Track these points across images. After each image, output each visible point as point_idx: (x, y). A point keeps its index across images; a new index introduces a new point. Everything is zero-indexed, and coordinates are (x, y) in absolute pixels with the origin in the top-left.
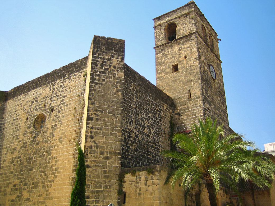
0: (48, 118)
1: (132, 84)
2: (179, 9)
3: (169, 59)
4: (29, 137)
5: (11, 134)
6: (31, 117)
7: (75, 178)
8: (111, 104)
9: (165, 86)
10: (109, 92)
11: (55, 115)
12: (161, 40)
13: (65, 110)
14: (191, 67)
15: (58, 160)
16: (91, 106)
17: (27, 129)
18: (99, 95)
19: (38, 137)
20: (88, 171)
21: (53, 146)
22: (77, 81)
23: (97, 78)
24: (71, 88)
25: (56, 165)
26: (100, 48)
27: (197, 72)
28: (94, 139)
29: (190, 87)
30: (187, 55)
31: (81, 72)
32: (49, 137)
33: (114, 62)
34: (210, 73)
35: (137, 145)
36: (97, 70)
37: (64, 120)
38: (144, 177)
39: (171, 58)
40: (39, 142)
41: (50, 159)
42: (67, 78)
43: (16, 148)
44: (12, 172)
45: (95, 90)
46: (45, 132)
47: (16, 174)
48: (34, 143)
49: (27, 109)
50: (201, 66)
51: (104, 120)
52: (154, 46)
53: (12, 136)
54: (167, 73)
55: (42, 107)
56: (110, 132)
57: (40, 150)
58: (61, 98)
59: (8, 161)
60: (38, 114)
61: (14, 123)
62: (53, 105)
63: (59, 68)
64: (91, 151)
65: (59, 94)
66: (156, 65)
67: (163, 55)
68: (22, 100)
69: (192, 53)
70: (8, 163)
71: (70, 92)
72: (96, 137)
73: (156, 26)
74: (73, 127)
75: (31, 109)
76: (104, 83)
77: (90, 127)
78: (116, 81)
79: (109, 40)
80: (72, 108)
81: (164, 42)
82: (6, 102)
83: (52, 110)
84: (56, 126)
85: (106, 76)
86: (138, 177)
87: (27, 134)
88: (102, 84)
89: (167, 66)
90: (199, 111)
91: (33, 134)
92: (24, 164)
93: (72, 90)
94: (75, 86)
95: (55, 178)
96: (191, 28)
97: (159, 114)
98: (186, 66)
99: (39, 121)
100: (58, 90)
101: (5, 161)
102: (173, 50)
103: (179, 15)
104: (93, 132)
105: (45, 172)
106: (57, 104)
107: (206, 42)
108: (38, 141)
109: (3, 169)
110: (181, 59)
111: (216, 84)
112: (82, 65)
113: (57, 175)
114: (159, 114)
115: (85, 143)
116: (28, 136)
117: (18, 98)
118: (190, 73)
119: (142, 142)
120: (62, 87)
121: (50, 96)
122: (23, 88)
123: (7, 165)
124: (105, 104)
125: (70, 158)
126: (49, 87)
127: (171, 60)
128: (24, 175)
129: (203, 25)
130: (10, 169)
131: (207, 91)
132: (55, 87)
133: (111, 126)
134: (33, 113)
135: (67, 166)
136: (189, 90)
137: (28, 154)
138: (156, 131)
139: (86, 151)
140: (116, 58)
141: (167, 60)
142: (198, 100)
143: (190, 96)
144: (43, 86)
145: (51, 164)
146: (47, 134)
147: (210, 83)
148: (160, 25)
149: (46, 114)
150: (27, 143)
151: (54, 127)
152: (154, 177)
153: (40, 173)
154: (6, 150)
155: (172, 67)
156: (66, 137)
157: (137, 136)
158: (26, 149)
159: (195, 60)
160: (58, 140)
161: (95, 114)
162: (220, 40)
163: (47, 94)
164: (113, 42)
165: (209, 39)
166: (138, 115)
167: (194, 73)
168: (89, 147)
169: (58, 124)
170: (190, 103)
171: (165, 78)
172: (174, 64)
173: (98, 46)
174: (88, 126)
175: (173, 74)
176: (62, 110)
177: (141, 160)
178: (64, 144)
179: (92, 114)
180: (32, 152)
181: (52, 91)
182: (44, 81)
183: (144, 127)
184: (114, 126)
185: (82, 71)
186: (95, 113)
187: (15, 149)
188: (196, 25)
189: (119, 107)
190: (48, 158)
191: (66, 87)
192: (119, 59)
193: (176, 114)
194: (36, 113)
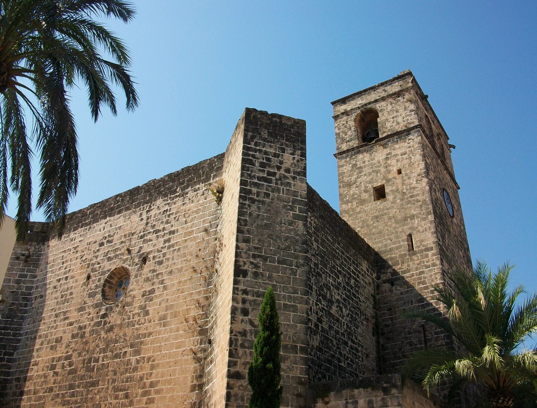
0: (136, 276)
1: (309, 213)
2: (382, 84)
3: (365, 175)
4: (91, 316)
5: (52, 310)
6: (97, 275)
7: (197, 404)
8: (282, 243)
9: (359, 227)
10: (279, 219)
11: (150, 271)
12: (349, 141)
13: (173, 259)
14: (412, 191)
15: (158, 365)
16: (243, 245)
17: (86, 299)
18: (258, 225)
19: (112, 315)
20: (239, 386)
21: (145, 334)
22: (201, 202)
23: (254, 190)
24: (187, 215)
25: (153, 375)
26: (257, 132)
27: (425, 200)
28: (250, 317)
29: (411, 228)
30: (403, 167)
31: (210, 184)
32: (136, 316)
33: (287, 161)
34: (444, 205)
35: (321, 338)
36: (253, 174)
37: (172, 280)
38: (364, 400)
39: (370, 174)
40: (113, 326)
41: (138, 362)
42: (179, 196)
43: (61, 337)
44: (51, 390)
45: (251, 214)
46: (128, 304)
47: (58, 394)
48: (104, 328)
49: (89, 257)
50: (430, 189)
51: (270, 277)
52: (336, 152)
53: (54, 313)
54: (362, 202)
55: (122, 254)
56: (282, 302)
57: (116, 341)
58: (164, 235)
59: (42, 366)
60: (113, 267)
61: (58, 287)
62: (146, 248)
63: (162, 176)
64: (244, 341)
65: (161, 228)
66: (340, 187)
67: (352, 168)
68: (77, 240)
69: (413, 164)
70: (43, 370)
71: (186, 222)
72: (254, 311)
73: (338, 116)
74: (192, 294)
75: (96, 257)
76: (267, 200)
77: (241, 290)
78: (291, 198)
79: (276, 119)
80: (191, 255)
81: (355, 143)
82: (43, 244)
83: (144, 260)
84: (152, 291)
85: (270, 186)
86: (350, 401)
87: (87, 309)
88: (263, 203)
89: (362, 189)
90: (431, 276)
91: (100, 310)
92: (78, 373)
93: (189, 219)
94: (196, 212)
95: (150, 403)
96: (408, 119)
97: (356, 280)
98: (400, 189)
99: (114, 283)
100: (159, 220)
101: (36, 364)
102: (374, 159)
103: (383, 94)
104: (248, 302)
105: (125, 390)
106: (156, 248)
107: (434, 146)
108: (111, 324)
109: (31, 381)
110: (390, 176)
111: (455, 227)
112: (211, 169)
113: (154, 398)
114: (356, 280)
115: (232, 323)
116: (90, 314)
117: (69, 236)
118: (409, 202)
119: (329, 333)
120: (168, 213)
121: (140, 232)
122: (82, 217)
123: (41, 373)
124: (270, 244)
125: (185, 360)
126: (139, 214)
127: (371, 177)
128: (77, 396)
129: (426, 117)
130: (45, 382)
131: (443, 237)
132: (152, 213)
133: (284, 289)
134: (102, 267)
135: (179, 378)
136: (410, 236)
137: (88, 352)
138: (352, 312)
139: (234, 341)
140: (291, 154)
141: (362, 177)
142: (430, 253)
143: (411, 246)
144: (125, 211)
145: (140, 373)
146: (131, 310)
147: (446, 222)
148: (346, 113)
149: (130, 268)
150: (87, 327)
151: (149, 295)
152: (388, 399)
153: (114, 391)
154: (40, 342)
155: (372, 191)
156: (175, 315)
157: (320, 320)
158: (84, 340)
159: (419, 178)
160: (157, 322)
161: (252, 263)
162: (454, 147)
163: (134, 227)
164: (283, 122)
165: (437, 142)
166: (321, 276)
167: (418, 201)
168: (240, 333)
169: (159, 288)
170: (412, 260)
171: (360, 212)
172: (375, 185)
173: (254, 129)
174: (237, 288)
175: (376, 204)
176: (168, 259)
177: (328, 369)
178: (171, 331)
179: (245, 263)
180: (98, 346)
181: (144, 222)
182: (128, 201)
183: (332, 303)
184: (290, 290)
185: (211, 181)
186: (252, 260)
187: (58, 340)
188: (417, 114)
189: (300, 252)
190: (133, 359)
191: (176, 214)
192: (296, 156)
193: (385, 282)
194: (110, 266)
